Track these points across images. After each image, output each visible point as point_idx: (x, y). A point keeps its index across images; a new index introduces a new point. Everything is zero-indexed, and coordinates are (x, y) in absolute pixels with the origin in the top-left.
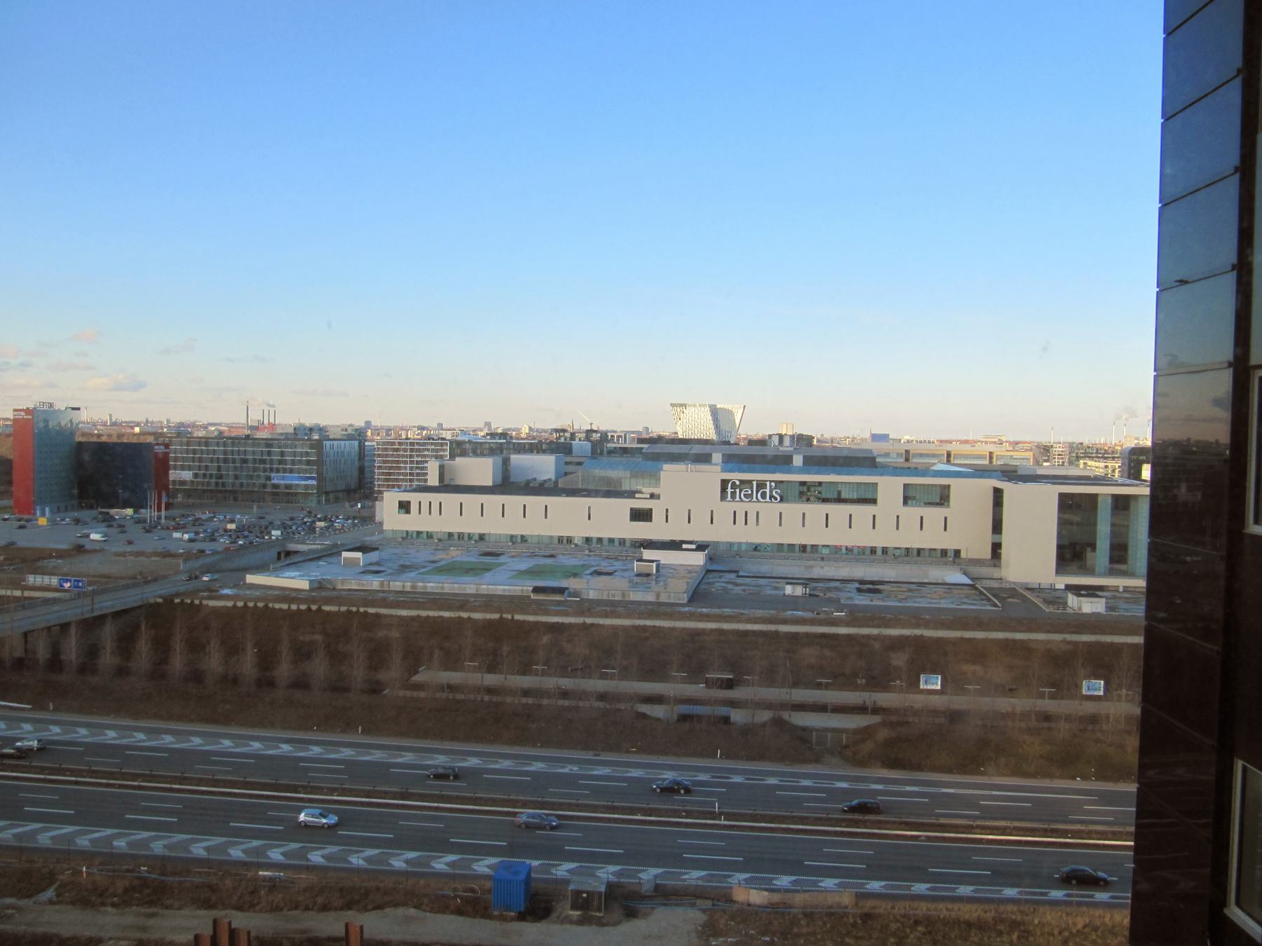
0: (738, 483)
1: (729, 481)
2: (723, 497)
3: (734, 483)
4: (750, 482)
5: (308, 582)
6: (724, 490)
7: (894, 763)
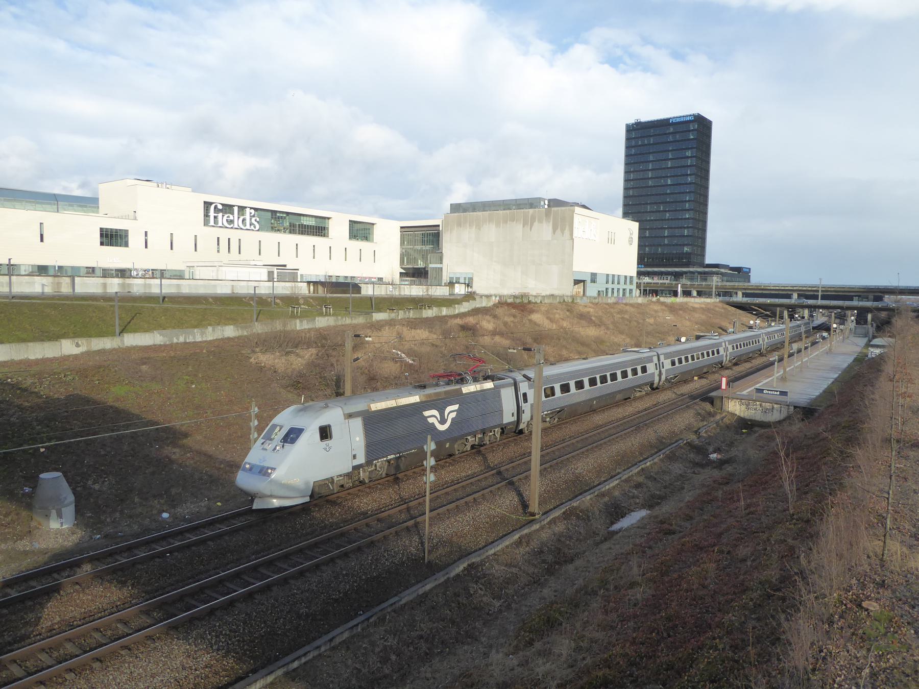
0: (220, 207)
1: (211, 204)
2: (206, 223)
3: (216, 207)
4: (231, 207)
5: (708, 261)
6: (206, 215)
7: (632, 588)
